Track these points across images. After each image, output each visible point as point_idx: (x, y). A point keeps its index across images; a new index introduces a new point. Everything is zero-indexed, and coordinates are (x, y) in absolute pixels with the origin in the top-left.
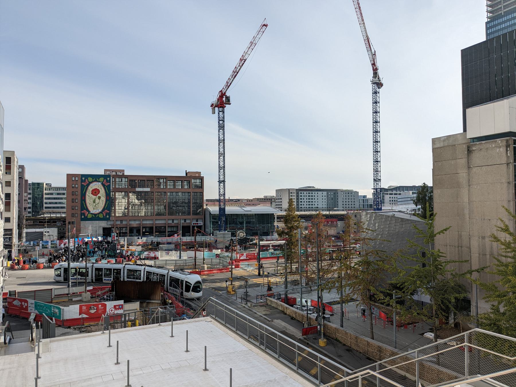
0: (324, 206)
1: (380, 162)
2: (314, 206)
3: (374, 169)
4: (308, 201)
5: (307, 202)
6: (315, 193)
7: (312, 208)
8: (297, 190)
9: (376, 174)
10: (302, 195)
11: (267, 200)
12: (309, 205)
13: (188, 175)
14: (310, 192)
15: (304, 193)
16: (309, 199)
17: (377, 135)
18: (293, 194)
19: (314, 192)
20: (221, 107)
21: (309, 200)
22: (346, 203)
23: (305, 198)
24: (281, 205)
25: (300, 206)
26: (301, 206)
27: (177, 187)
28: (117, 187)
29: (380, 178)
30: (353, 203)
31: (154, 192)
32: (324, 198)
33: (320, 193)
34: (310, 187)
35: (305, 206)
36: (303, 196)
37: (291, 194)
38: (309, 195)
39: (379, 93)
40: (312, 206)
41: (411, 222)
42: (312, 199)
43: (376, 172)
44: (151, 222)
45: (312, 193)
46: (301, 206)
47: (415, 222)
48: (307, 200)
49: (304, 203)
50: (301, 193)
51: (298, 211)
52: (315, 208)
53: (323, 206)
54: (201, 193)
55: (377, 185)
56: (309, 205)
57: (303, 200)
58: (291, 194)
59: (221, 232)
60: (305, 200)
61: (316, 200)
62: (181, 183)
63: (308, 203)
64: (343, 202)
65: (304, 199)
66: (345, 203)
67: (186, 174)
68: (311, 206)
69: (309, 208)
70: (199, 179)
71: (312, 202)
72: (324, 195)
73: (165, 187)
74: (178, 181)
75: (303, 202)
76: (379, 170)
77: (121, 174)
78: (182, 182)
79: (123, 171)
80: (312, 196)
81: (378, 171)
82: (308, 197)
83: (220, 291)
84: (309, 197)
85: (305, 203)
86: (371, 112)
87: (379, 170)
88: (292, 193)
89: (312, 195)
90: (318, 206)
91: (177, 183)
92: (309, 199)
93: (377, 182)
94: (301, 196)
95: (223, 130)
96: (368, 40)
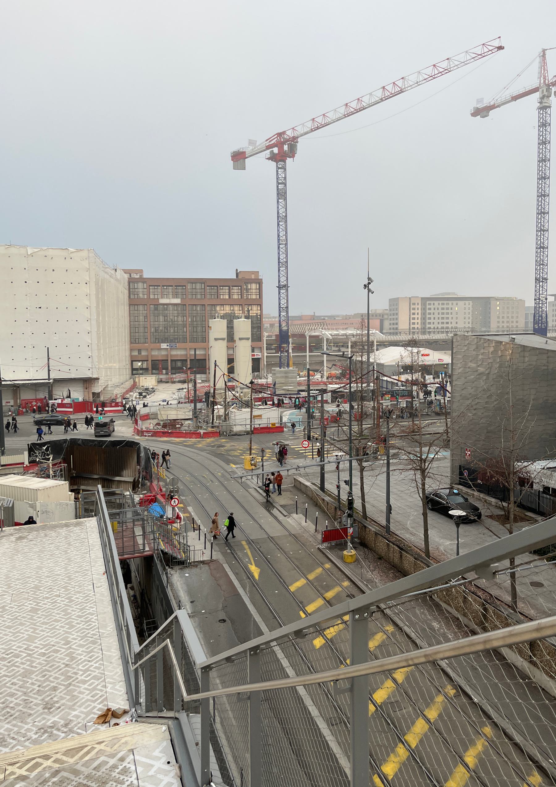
0: (467, 325)
1: (547, 248)
2: (450, 326)
3: (536, 261)
4: (440, 316)
5: (439, 318)
6: (452, 304)
7: (447, 328)
8: (422, 298)
9: (540, 269)
10: (432, 307)
11: (376, 316)
12: (443, 323)
13: (240, 277)
14: (445, 302)
15: (434, 304)
16: (443, 314)
17: (544, 201)
18: (416, 306)
19: (450, 302)
20: (280, 161)
21: (443, 316)
22: (503, 320)
23: (436, 312)
24: (397, 324)
25: (428, 326)
26: (429, 326)
27: (222, 297)
28: (152, 297)
29: (546, 276)
30: (514, 320)
31: (187, 306)
32: (467, 311)
33: (461, 303)
34: (449, 294)
35: (436, 325)
36: (440, 309)
37: (412, 306)
38: (443, 306)
39: (550, 125)
40: (447, 325)
41: (540, 353)
42: (448, 313)
43: (540, 265)
44: (183, 352)
45: (448, 304)
46: (429, 326)
47: (547, 352)
48: (439, 316)
49: (434, 321)
50: (430, 304)
51: (424, 333)
52: (434, 328)
53: (464, 325)
54: (185, 306)
55: (541, 289)
56: (443, 323)
57: (432, 316)
58: (412, 306)
59: (282, 369)
60: (436, 316)
61: (454, 316)
62: (227, 291)
63: (440, 321)
64: (498, 317)
65: (434, 314)
66: (501, 320)
67: (237, 275)
68: (445, 325)
69: (442, 328)
70: (256, 283)
71: (448, 318)
72: (467, 306)
73: (203, 297)
74: (223, 286)
75: (432, 318)
76: (546, 262)
77: (138, 277)
78: (229, 289)
79: (141, 271)
80: (448, 309)
81: (543, 265)
82: (440, 311)
83: (235, 465)
84: (443, 311)
85: (436, 321)
86: (536, 159)
87: (546, 262)
88: (414, 304)
89: (447, 306)
90: (456, 325)
91: (221, 291)
92: (443, 314)
93: (541, 283)
94: (430, 309)
95: (285, 199)
96: (515, 98)
